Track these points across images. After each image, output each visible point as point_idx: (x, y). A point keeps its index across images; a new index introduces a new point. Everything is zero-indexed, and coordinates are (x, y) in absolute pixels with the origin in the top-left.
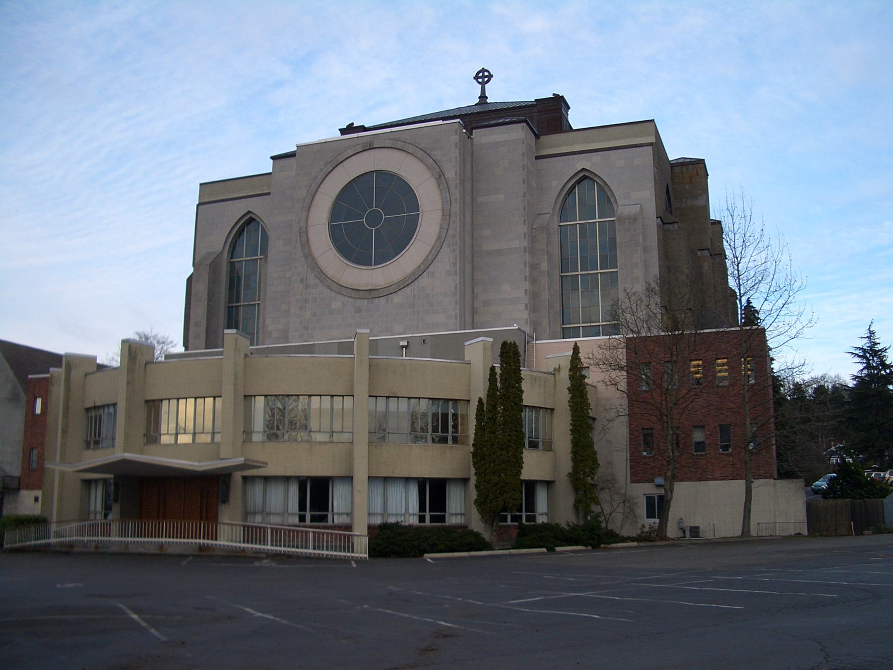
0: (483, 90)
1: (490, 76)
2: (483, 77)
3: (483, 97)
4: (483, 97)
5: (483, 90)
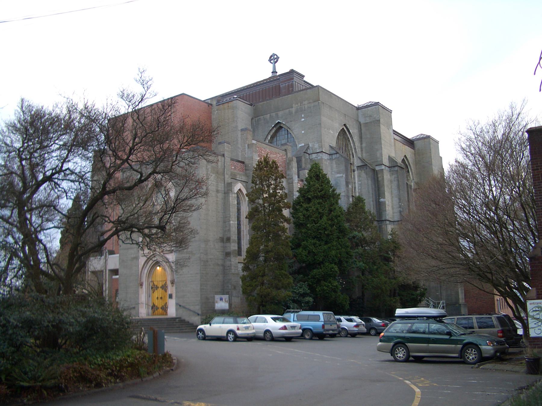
0: (274, 68)
1: (278, 58)
2: (274, 59)
3: (274, 72)
4: (274, 72)
5: (274, 68)
